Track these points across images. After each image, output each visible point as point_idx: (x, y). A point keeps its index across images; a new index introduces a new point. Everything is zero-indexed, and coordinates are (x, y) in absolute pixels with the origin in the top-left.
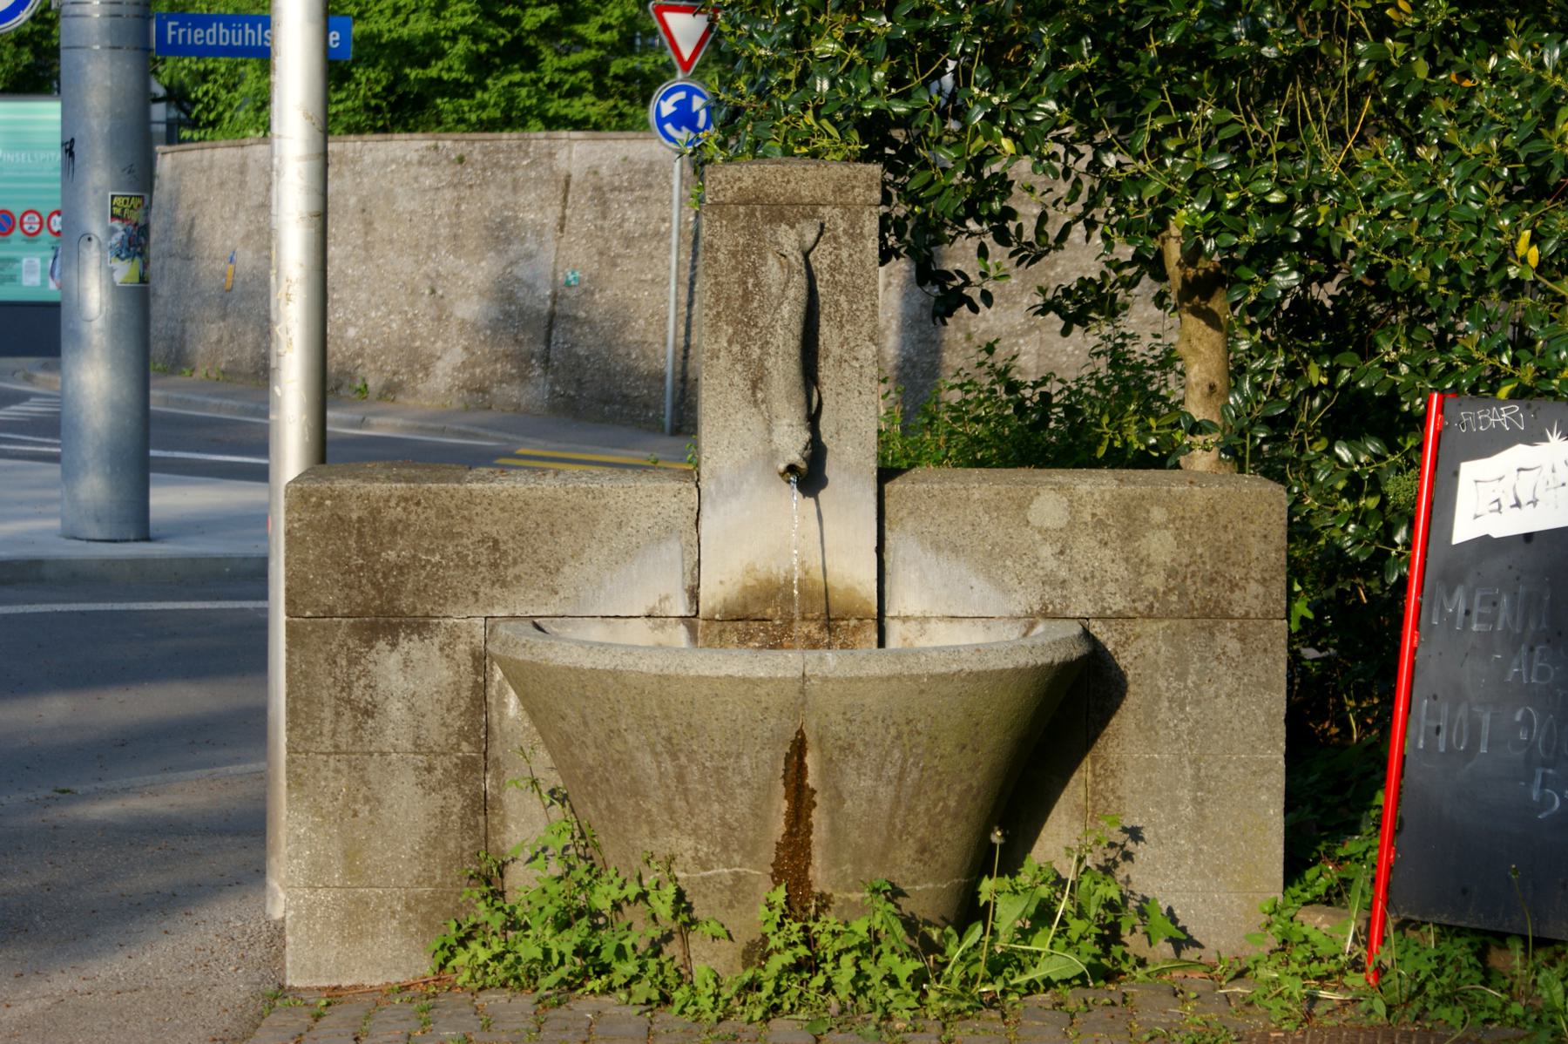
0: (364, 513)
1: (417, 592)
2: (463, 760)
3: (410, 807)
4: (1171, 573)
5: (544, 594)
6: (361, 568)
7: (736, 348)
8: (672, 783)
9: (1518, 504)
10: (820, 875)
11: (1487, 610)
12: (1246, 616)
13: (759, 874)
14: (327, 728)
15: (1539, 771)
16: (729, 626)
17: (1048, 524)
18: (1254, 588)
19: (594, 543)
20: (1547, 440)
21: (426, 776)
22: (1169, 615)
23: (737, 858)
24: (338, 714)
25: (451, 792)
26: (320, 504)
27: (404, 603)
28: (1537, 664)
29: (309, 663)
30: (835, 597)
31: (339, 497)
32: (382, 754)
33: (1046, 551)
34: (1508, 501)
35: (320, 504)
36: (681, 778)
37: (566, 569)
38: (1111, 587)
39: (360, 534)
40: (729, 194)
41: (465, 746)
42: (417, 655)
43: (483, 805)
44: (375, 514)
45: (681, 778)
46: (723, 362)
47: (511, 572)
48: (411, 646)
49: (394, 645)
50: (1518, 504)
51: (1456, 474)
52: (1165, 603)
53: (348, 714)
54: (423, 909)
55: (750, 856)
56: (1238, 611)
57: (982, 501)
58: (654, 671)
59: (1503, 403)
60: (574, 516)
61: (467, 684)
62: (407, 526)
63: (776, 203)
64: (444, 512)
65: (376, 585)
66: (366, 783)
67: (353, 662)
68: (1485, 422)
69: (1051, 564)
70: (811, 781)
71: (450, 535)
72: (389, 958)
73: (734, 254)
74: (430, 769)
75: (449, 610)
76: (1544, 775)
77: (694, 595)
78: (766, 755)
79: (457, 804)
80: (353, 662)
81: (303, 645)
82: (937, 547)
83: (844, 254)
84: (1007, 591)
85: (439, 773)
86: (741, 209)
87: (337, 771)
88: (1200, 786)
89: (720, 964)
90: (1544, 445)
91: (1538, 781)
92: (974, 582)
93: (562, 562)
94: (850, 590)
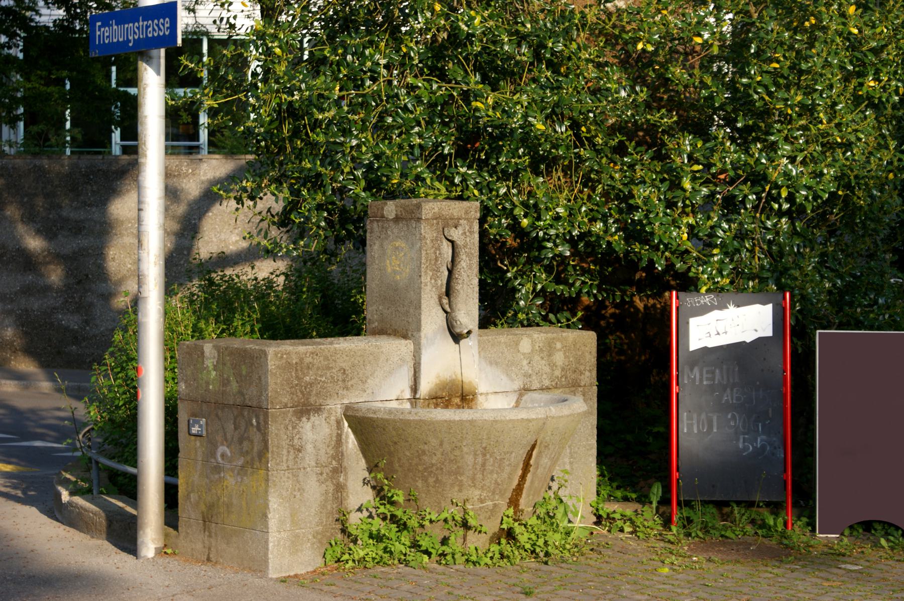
0: (297, 360)
1: (317, 394)
2: (333, 468)
3: (314, 490)
4: (563, 369)
6: (297, 385)
7: (433, 281)
8: (478, 467)
9: (718, 334)
10: (523, 502)
11: (710, 376)
12: (585, 386)
13: (503, 503)
14: (285, 458)
15: (741, 437)
16: (431, 401)
17: (526, 351)
18: (587, 374)
19: (378, 369)
20: (727, 308)
21: (320, 477)
22: (562, 386)
23: (497, 497)
24: (289, 452)
25: (329, 483)
26: (282, 357)
27: (312, 400)
28: (735, 396)
29: (278, 430)
30: (465, 386)
32: (304, 468)
33: (525, 362)
34: (713, 333)
35: (282, 357)
36: (484, 465)
37: (369, 381)
38: (545, 376)
39: (297, 370)
41: (334, 463)
42: (317, 422)
43: (340, 488)
44: (301, 360)
45: (484, 465)
46: (429, 287)
47: (350, 383)
48: (314, 418)
49: (309, 419)
50: (718, 334)
51: (688, 323)
52: (561, 381)
53: (292, 451)
54: (319, 537)
55: (502, 495)
56: (583, 383)
57: (505, 343)
58: (491, 419)
59: (704, 295)
60: (371, 357)
61: (335, 435)
62: (313, 365)
63: (446, 219)
65: (302, 392)
66: (298, 482)
67: (294, 428)
68: (699, 302)
69: (526, 368)
70: (532, 462)
72: (307, 560)
73: (432, 241)
74: (321, 474)
75: (328, 402)
76: (744, 438)
77: (415, 389)
78: (521, 452)
79: (331, 488)
80: (294, 428)
81: (276, 422)
82: (491, 363)
83: (468, 239)
84: (513, 380)
85: (325, 475)
87: (288, 478)
88: (571, 457)
89: (479, 544)
90: (726, 310)
91: (741, 440)
92: (502, 377)
93: (367, 377)
94: (470, 382)
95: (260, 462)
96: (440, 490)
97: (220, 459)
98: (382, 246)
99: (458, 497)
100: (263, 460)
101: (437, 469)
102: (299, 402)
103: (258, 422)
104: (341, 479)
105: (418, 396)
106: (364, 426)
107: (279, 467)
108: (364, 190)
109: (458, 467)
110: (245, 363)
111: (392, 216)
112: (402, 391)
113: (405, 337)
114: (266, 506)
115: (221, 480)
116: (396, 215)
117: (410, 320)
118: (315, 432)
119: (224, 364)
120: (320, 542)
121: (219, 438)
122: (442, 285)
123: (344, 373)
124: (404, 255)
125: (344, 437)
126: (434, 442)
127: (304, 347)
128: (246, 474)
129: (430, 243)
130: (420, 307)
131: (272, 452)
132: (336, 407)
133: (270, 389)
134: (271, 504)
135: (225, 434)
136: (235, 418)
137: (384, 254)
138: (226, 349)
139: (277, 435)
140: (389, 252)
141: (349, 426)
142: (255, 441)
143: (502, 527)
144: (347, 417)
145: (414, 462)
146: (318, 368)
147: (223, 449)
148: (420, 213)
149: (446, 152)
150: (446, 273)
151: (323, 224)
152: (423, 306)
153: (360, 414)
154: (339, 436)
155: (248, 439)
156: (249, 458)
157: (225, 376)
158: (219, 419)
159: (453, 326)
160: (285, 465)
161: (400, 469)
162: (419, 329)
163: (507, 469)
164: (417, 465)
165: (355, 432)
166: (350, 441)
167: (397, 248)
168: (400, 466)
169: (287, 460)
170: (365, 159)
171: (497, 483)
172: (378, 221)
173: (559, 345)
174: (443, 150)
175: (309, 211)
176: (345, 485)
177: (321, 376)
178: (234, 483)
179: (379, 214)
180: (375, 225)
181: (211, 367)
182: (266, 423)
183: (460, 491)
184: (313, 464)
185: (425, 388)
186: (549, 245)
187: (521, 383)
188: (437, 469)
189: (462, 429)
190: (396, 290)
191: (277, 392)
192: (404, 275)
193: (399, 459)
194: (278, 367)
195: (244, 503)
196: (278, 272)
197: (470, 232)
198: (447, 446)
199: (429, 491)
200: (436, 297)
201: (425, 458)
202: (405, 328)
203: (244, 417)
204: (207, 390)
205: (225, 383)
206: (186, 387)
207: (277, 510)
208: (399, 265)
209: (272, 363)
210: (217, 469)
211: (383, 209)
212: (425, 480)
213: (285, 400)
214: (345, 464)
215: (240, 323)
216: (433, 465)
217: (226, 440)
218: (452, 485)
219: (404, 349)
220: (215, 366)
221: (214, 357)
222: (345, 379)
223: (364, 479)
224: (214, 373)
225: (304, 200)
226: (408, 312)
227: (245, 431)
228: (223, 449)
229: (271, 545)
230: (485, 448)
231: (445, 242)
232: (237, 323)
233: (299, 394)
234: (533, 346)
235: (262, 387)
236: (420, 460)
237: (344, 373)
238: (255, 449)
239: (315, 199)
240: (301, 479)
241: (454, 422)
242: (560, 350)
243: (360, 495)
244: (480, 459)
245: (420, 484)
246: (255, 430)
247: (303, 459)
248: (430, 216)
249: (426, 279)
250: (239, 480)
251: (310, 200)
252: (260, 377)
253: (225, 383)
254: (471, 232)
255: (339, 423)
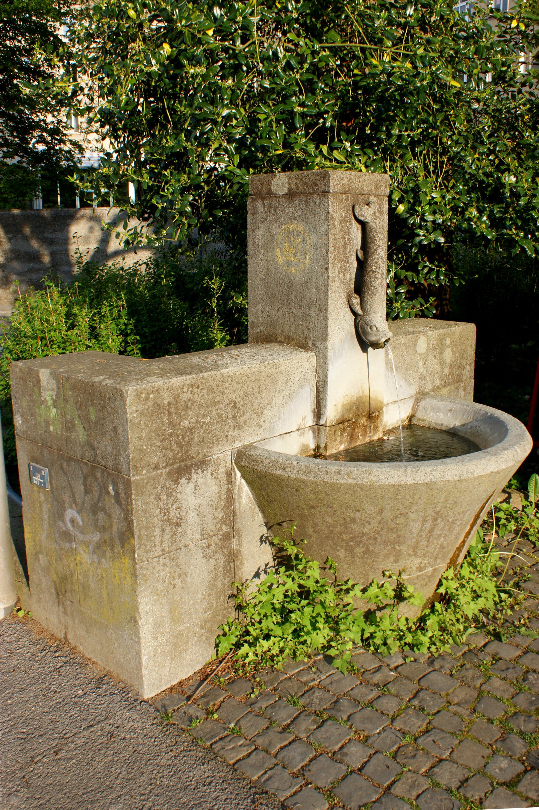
0: (170, 399)
1: (201, 442)
2: (223, 535)
3: (200, 570)
4: (451, 366)
5: (256, 429)
6: (171, 435)
7: (341, 275)
8: (424, 534)
14: (158, 540)
18: (468, 367)
21: (208, 551)
22: (449, 384)
24: (163, 530)
26: (147, 398)
30: (372, 402)
31: (157, 391)
33: (421, 363)
35: (147, 398)
36: (431, 531)
37: (265, 412)
39: (170, 414)
40: (339, 187)
42: (201, 481)
43: (233, 558)
44: (176, 398)
45: (431, 531)
46: (337, 284)
48: (198, 477)
49: (189, 479)
52: (448, 379)
53: (168, 528)
54: (208, 625)
57: (405, 344)
60: (268, 381)
64: (211, 390)
65: (179, 444)
66: (178, 566)
67: (169, 496)
69: (422, 370)
71: (214, 403)
73: (341, 222)
74: (208, 547)
75: (216, 449)
77: (318, 413)
79: (221, 559)
80: (169, 496)
81: (143, 493)
84: (410, 385)
86: (344, 196)
93: (264, 408)
95: (123, 546)
96: (369, 561)
97: (69, 525)
98: (269, 230)
99: (392, 567)
100: (127, 546)
101: (369, 539)
102: (175, 459)
103: (117, 493)
104: (234, 546)
105: (322, 422)
106: (266, 483)
107: (151, 555)
108: (239, 166)
109: (399, 536)
110: (93, 404)
111: (284, 191)
112: (304, 418)
113: (304, 346)
114: (136, 609)
115: (72, 551)
116: (290, 189)
117: (311, 326)
118: (198, 495)
119: (66, 401)
120: (210, 631)
121: (66, 497)
122: (350, 280)
123: (235, 407)
124: (303, 241)
125: (236, 491)
126: (370, 509)
127: (180, 379)
128: (104, 555)
129: (327, 224)
130: (326, 310)
131: (140, 537)
132: (224, 454)
133: (131, 447)
134: (141, 607)
135: (74, 496)
136: (85, 479)
137: (272, 240)
138: (67, 379)
139: (144, 511)
140: (279, 238)
141: (243, 476)
142: (114, 516)
143: (439, 591)
144: (241, 468)
145: (337, 530)
146: (200, 406)
147: (70, 513)
148: (327, 185)
149: (328, 124)
150: (355, 264)
151: (188, 209)
152: (331, 308)
153: (260, 468)
154: (230, 493)
155: (104, 510)
156: (107, 537)
157: (68, 417)
158: (65, 473)
159: (365, 333)
160: (159, 549)
161: (314, 535)
162: (324, 338)
163: (457, 529)
164: (340, 533)
165: (251, 484)
166: (244, 495)
167: (291, 233)
168: (315, 532)
169: (162, 542)
170: (236, 133)
171: (442, 547)
172: (263, 199)
173: (448, 342)
174: (324, 123)
175: (172, 194)
176: (239, 551)
177: (205, 416)
178: (89, 561)
179: (264, 190)
180: (259, 204)
181: (50, 403)
182: (128, 496)
183: (396, 561)
184: (198, 536)
185: (331, 414)
186: (421, 232)
187: (417, 387)
188: (369, 539)
189: (414, 494)
190: (289, 287)
191: (142, 451)
192: (302, 267)
193: (315, 525)
194: (142, 413)
195: (104, 592)
196: (141, 262)
197: (380, 212)
198: (388, 514)
199: (353, 562)
200: (344, 296)
201: (355, 526)
202: (306, 337)
203: (96, 479)
204: (47, 431)
205: (69, 427)
206: (23, 422)
207: (149, 608)
208: (294, 255)
209: (132, 409)
210: (67, 536)
211: (269, 183)
212: (350, 550)
213: (154, 460)
214: (238, 525)
215: (108, 309)
216: (363, 534)
217: (75, 502)
218: (387, 556)
219: (305, 364)
220: (55, 401)
221: (53, 390)
222: (237, 415)
223: (261, 537)
224: (54, 411)
225: (167, 183)
226: (307, 315)
227: (99, 498)
228: (70, 513)
229: (144, 659)
230: (438, 513)
231: (354, 223)
232: (105, 309)
233: (176, 448)
234: (428, 344)
235: (120, 445)
236: (346, 528)
237: (235, 407)
238: (115, 528)
239: (179, 181)
240: (181, 561)
241: (405, 486)
242: (449, 346)
243: (256, 555)
244: (428, 526)
245: (342, 553)
246: (113, 500)
247: (184, 534)
248: (338, 188)
249: (333, 272)
250: (96, 560)
251: (173, 182)
252: (115, 427)
253: (69, 427)
254: (381, 213)
255: (229, 475)
